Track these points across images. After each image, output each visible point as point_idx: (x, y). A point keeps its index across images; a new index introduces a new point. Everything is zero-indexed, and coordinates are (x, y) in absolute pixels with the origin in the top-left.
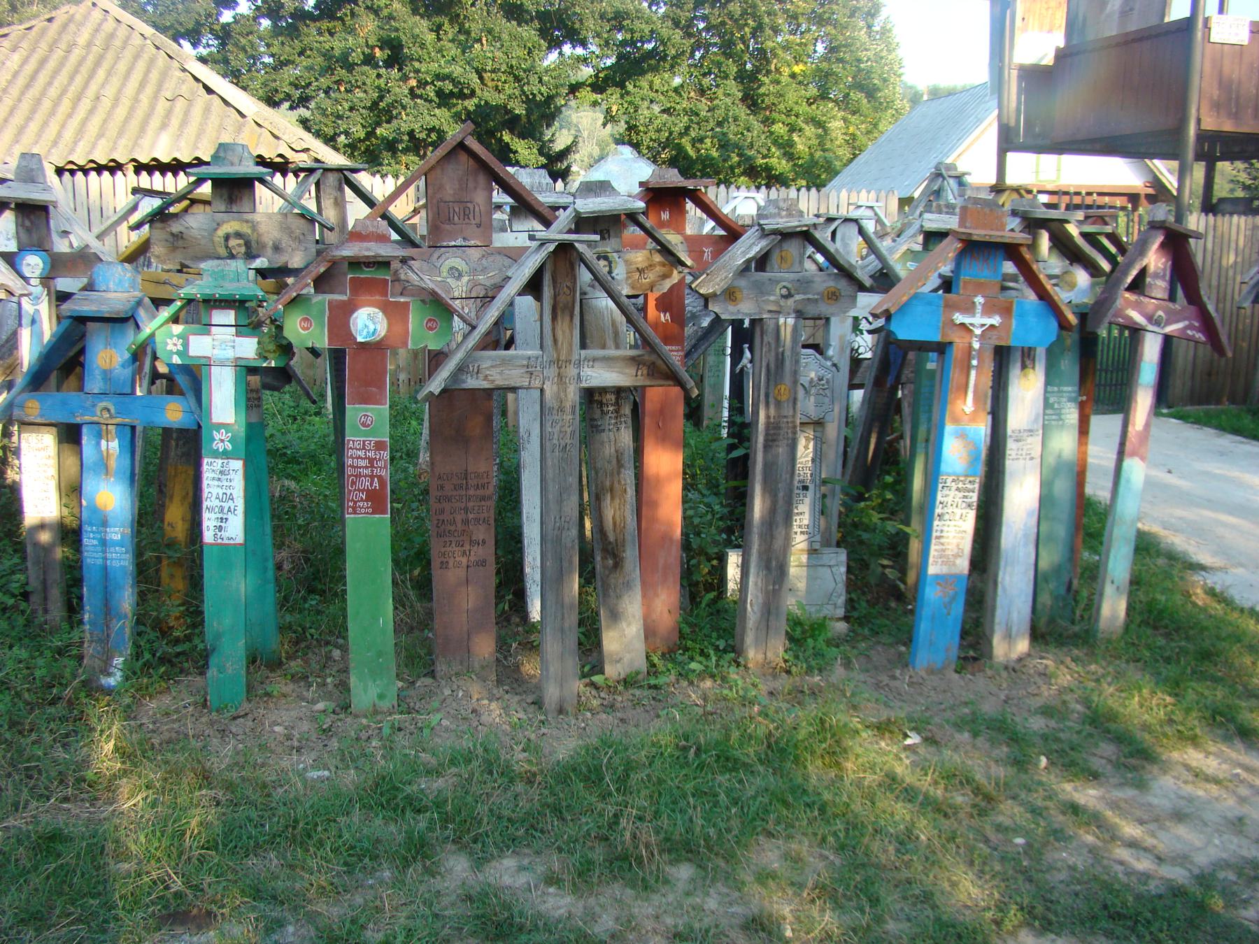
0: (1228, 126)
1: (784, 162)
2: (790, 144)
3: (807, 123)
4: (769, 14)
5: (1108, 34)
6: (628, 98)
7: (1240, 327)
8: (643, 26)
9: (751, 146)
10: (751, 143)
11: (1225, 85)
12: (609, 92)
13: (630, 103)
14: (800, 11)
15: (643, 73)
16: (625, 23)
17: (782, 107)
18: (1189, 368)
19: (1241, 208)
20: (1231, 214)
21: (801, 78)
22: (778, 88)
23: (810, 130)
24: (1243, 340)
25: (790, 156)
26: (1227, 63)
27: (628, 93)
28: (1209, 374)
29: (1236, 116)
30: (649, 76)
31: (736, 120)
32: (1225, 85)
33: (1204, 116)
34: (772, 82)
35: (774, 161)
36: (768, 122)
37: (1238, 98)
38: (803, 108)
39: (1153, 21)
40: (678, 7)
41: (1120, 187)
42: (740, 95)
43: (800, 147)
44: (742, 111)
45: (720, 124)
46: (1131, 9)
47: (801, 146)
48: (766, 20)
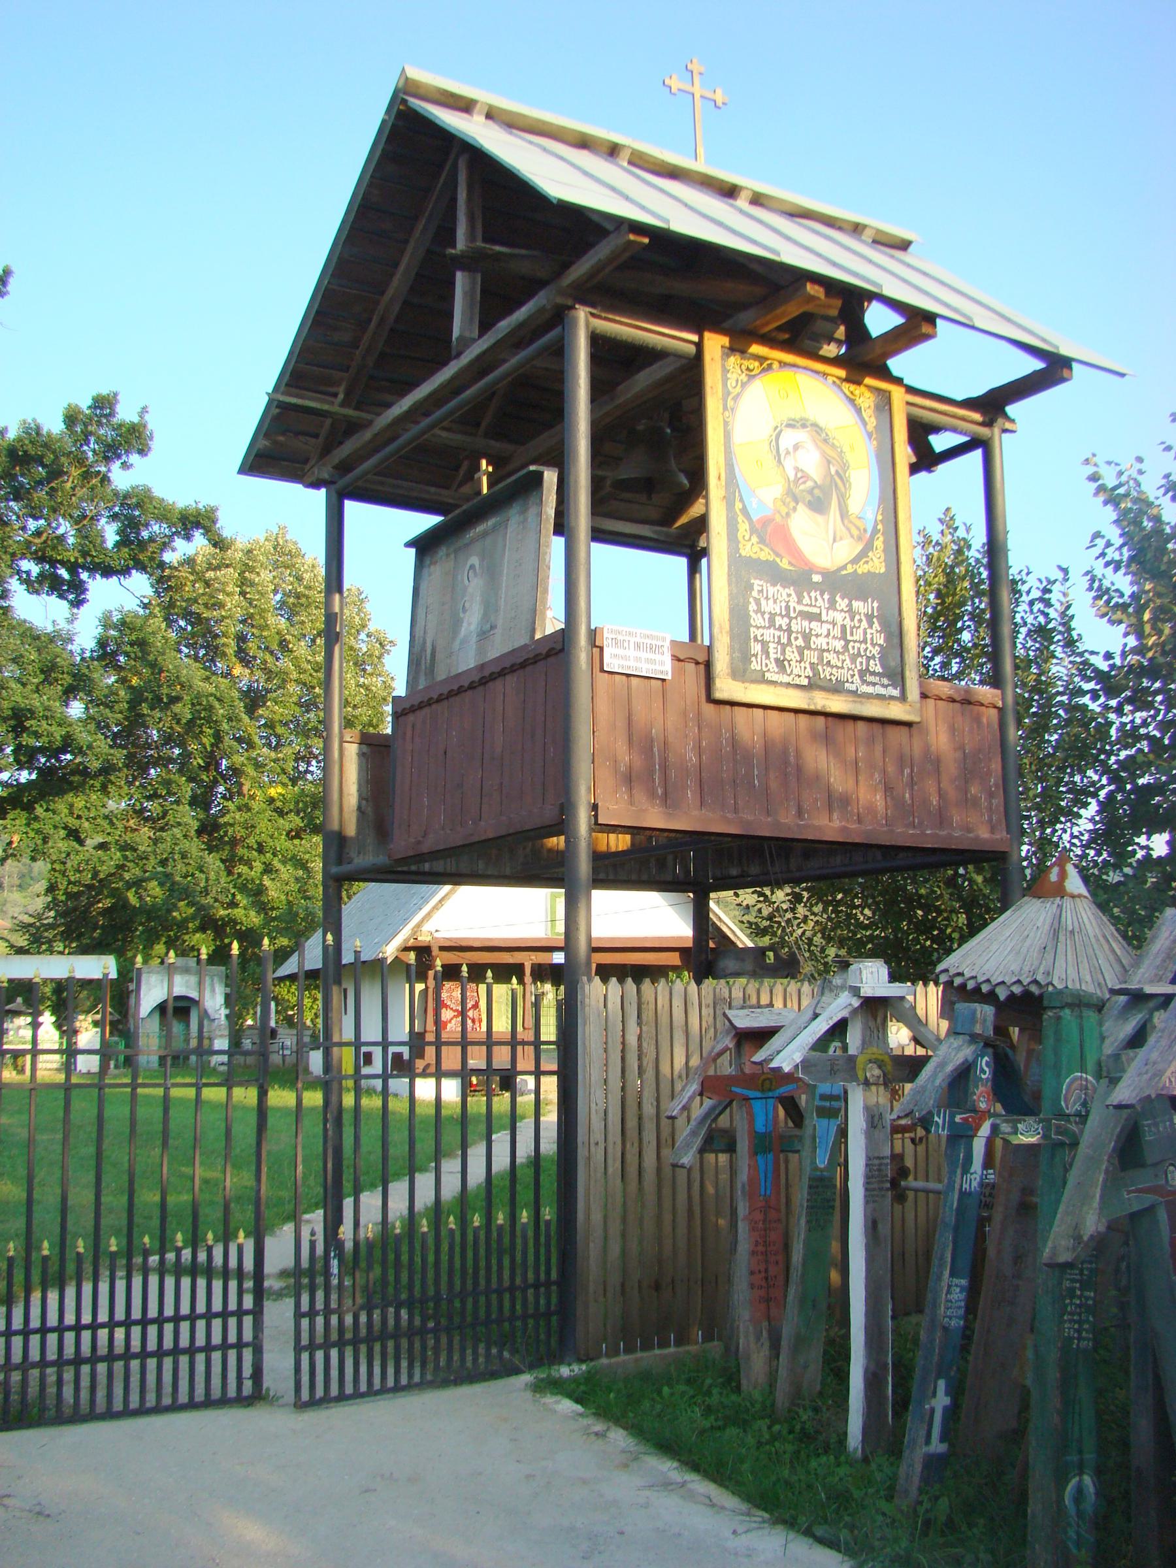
0: (655, 818)
1: (253, 913)
2: (260, 891)
3: (284, 863)
4: (230, 719)
5: (462, 668)
6: (36, 825)
7: (711, 1190)
8: (54, 728)
9: (206, 892)
10: (206, 888)
11: (644, 743)
12: (10, 816)
13: (38, 832)
14: (277, 717)
15: (61, 792)
16: (27, 724)
17: (251, 841)
18: (615, 1279)
19: (749, 966)
20: (737, 975)
21: (279, 804)
22: (247, 816)
23: (287, 872)
24: (718, 1214)
25: (263, 907)
26: (639, 707)
27: (36, 819)
28: (657, 1287)
29: (667, 799)
30: (70, 797)
31: (184, 856)
32: (644, 743)
33: (604, 802)
34: (239, 809)
35: (238, 913)
36: (229, 864)
37: (665, 768)
38: (283, 843)
39: (523, 640)
40: (107, 706)
41: (645, 939)
42: (195, 825)
43: (273, 893)
44: (195, 847)
45: (163, 863)
46: (492, 627)
47: (274, 891)
48: (225, 726)
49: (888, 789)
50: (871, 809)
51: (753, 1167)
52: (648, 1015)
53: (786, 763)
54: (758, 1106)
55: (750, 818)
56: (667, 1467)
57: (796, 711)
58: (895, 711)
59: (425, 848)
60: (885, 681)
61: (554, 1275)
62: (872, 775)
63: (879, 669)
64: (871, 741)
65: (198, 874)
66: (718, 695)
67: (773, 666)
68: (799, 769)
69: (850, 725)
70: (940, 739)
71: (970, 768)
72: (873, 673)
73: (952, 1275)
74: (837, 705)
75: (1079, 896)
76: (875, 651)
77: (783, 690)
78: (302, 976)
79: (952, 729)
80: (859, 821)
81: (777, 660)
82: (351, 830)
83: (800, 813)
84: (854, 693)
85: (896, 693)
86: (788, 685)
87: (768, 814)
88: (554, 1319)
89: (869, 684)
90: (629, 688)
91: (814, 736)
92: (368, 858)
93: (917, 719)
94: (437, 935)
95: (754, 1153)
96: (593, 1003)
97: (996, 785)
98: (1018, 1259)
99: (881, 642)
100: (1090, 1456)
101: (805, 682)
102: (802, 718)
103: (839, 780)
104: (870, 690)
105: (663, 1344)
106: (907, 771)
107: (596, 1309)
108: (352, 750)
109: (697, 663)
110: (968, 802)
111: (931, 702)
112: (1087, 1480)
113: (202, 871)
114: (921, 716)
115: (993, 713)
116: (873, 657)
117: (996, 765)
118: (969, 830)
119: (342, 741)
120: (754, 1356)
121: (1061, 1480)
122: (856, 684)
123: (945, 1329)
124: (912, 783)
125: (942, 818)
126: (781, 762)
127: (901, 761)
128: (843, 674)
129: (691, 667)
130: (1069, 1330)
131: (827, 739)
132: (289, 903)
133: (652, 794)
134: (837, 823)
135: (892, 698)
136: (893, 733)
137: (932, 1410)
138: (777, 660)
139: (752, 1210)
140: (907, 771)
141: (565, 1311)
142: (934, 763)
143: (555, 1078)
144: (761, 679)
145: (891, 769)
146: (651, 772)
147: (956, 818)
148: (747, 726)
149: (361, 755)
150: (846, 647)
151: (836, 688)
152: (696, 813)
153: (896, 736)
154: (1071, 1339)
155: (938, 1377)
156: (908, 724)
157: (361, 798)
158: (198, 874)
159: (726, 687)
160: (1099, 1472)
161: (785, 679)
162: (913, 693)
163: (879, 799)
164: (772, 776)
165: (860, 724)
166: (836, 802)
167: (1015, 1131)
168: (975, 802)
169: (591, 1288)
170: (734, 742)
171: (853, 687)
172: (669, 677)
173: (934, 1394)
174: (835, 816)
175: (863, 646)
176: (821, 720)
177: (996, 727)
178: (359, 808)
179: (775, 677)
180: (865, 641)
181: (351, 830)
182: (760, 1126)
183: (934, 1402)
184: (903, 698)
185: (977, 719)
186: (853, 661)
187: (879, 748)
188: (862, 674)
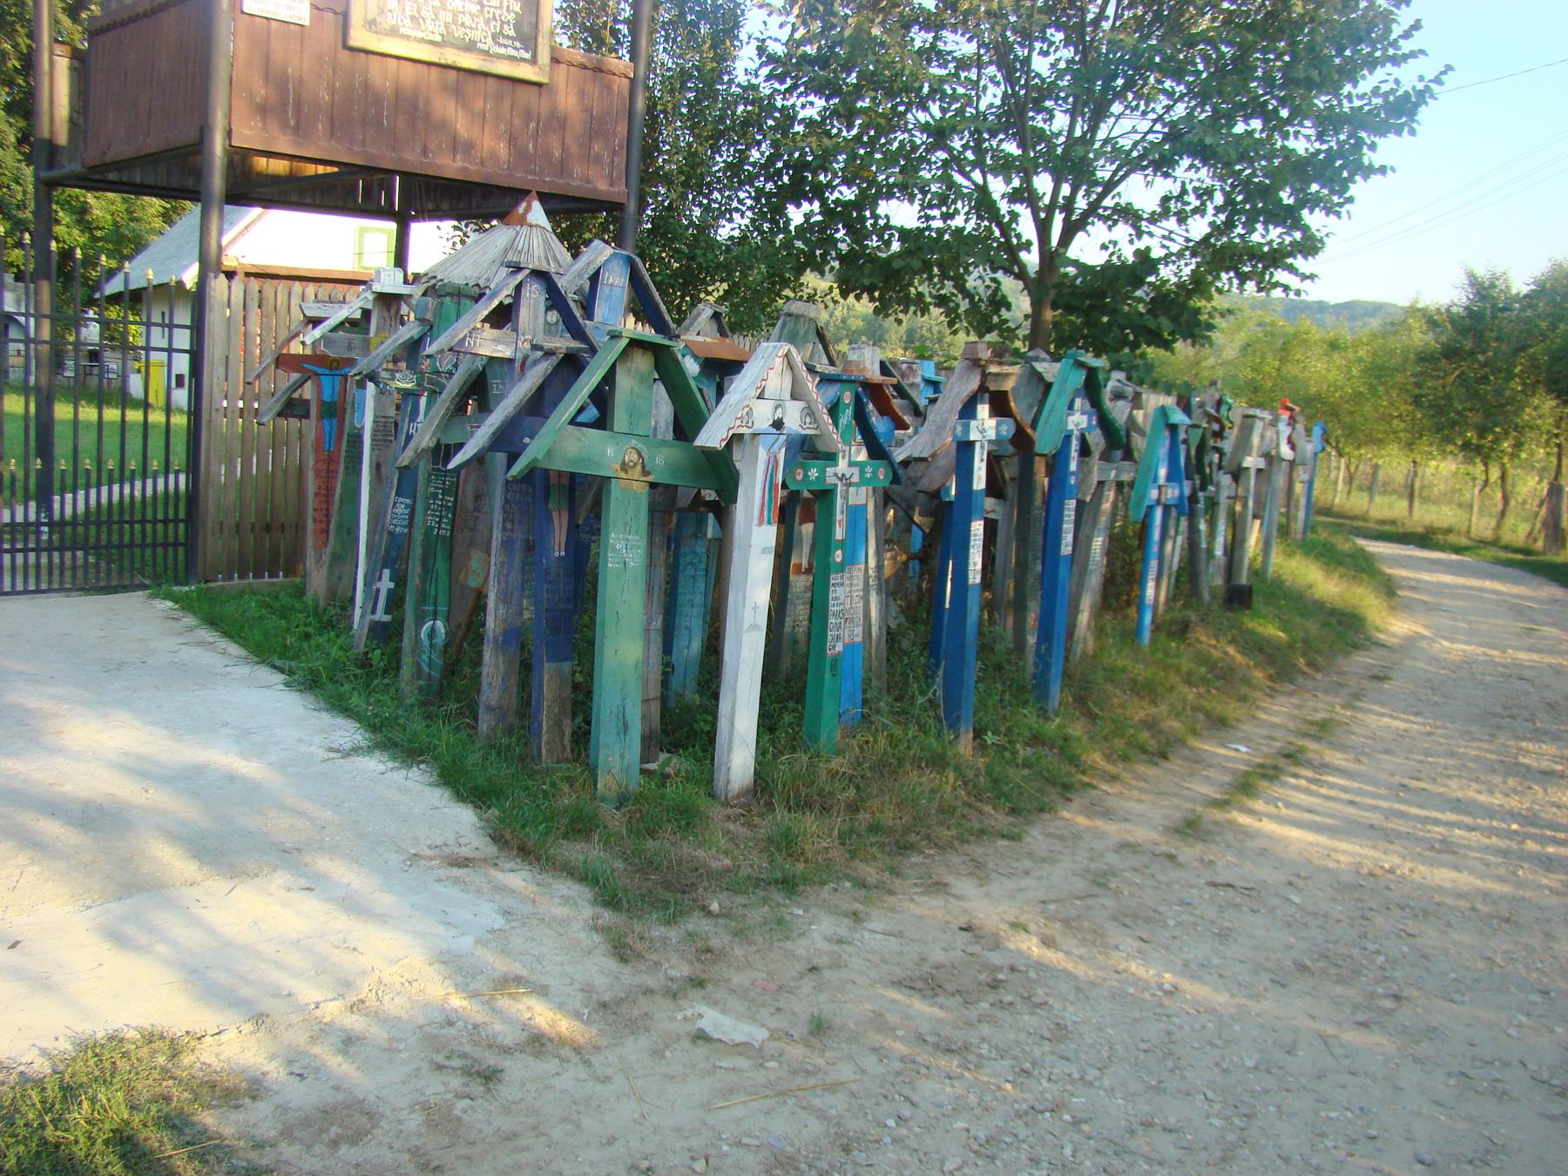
29: (299, 130)
37: (298, 104)
49: (512, 139)
50: (494, 156)
51: (320, 429)
52: (269, 306)
53: (415, 107)
54: (326, 381)
55: (374, 151)
56: (206, 634)
57: (429, 64)
58: (525, 72)
59: (108, 159)
60: (518, 45)
61: (182, 515)
62: (498, 125)
63: (512, 33)
64: (499, 98)
65: (13, 186)
66: (353, 43)
67: (408, 22)
68: (427, 116)
69: (482, 80)
70: (568, 101)
71: (595, 128)
72: (507, 37)
73: (398, 494)
74: (469, 61)
75: (537, 226)
76: (511, 17)
77: (416, 45)
78: (127, 296)
79: (582, 94)
80: (482, 164)
81: (412, 17)
82: (62, 138)
83: (425, 152)
84: (486, 53)
85: (527, 56)
86: (422, 41)
87: (394, 149)
88: (181, 550)
89: (500, 45)
90: (269, 29)
91: (445, 87)
92: (70, 167)
93: (545, 80)
94: (242, 261)
95: (321, 417)
96: (218, 295)
97: (620, 146)
98: (478, 497)
99: (518, 9)
100: (442, 609)
101: (439, 39)
102: (434, 70)
103: (462, 126)
104: (502, 51)
105: (273, 575)
106: (532, 125)
107: (214, 546)
108: (63, 64)
109: (336, 13)
110: (591, 159)
111: (563, 67)
112: (439, 624)
113: (18, 183)
114: (551, 78)
115: (625, 82)
116: (508, 23)
117: (622, 129)
118: (588, 182)
119: (52, 53)
120: (314, 574)
121: (419, 624)
122: (488, 45)
123: (391, 533)
124: (536, 136)
125: (562, 168)
126: (409, 109)
127: (528, 116)
128: (476, 35)
129: (329, 16)
130: (432, 521)
131: (457, 92)
132: (115, 223)
133: (284, 124)
134: (459, 164)
135: (523, 60)
136: (523, 91)
137: (378, 590)
138: (412, 17)
139: (317, 462)
140: (532, 125)
141: (191, 544)
142: (558, 122)
143: (187, 356)
144: (394, 32)
145: (516, 122)
146: (285, 105)
147: (577, 170)
148: (378, 74)
149: (73, 69)
150: (481, 11)
151: (470, 47)
152: (324, 143)
153: (525, 94)
154: (432, 528)
155: (384, 567)
156: (539, 85)
157: (73, 109)
158: (13, 186)
159: (359, 37)
160: (448, 620)
161: (420, 35)
162: (544, 57)
163: (502, 149)
164: (401, 118)
165: (491, 81)
166: (457, 145)
167: (393, 378)
168: (598, 159)
169: (210, 525)
170: (366, 85)
171: (486, 48)
172: (307, 23)
173: (380, 579)
174: (458, 157)
175: (498, 12)
176: (452, 75)
177: (626, 94)
178: (71, 120)
179: (409, 32)
180: (501, 8)
181: (62, 138)
182: (327, 397)
183: (379, 585)
184: (534, 61)
185: (608, 87)
186: (487, 22)
187: (507, 104)
188: (494, 37)
